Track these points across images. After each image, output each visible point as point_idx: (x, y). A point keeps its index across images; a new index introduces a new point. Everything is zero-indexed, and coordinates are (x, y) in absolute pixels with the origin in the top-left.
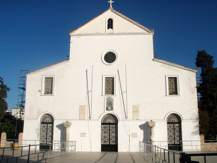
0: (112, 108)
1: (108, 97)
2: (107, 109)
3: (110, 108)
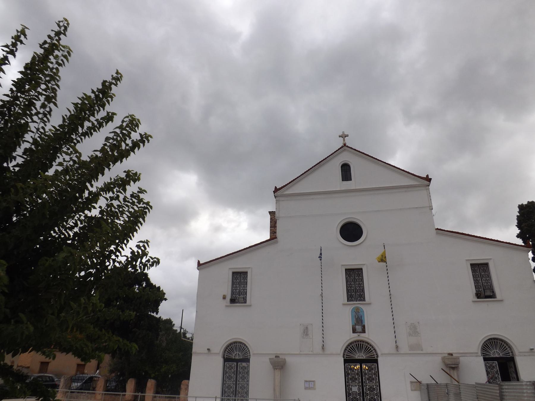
0: (364, 327)
1: (354, 306)
2: (354, 331)
3: (359, 328)
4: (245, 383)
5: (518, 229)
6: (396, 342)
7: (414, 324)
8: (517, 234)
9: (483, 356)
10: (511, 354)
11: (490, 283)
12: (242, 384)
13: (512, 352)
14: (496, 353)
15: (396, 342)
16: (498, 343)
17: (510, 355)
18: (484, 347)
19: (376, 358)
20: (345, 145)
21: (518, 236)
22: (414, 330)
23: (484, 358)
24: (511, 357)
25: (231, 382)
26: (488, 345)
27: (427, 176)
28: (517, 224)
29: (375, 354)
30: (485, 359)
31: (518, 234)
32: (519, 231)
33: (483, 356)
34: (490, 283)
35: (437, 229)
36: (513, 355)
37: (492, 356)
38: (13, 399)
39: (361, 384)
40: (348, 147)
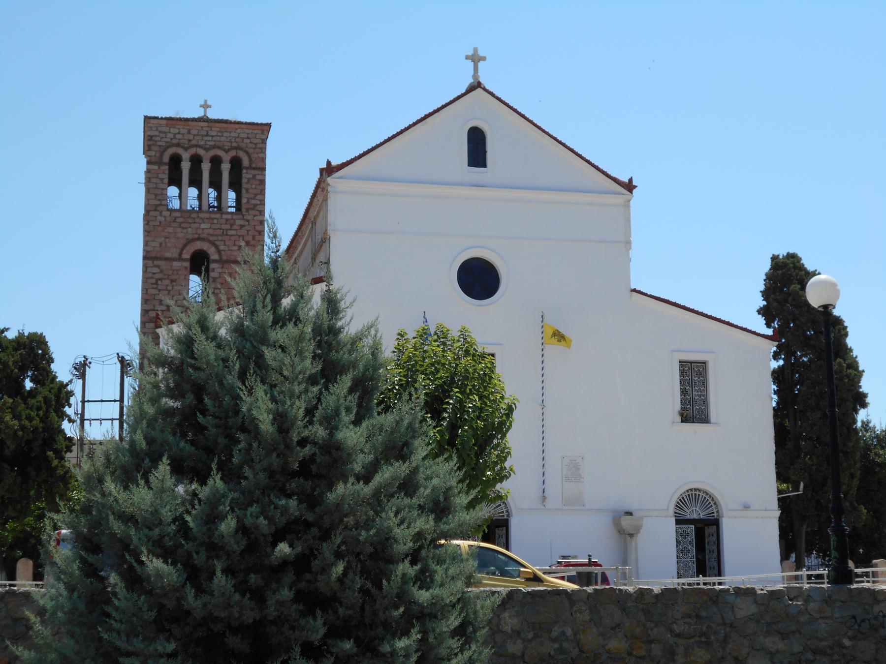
4: (689, 560)
5: (763, 298)
6: (544, 492)
7: (575, 461)
8: (758, 308)
9: (676, 516)
10: (715, 514)
11: (704, 415)
12: (688, 558)
13: (718, 512)
14: (695, 512)
15: (544, 492)
16: (700, 497)
17: (714, 516)
18: (678, 503)
19: (505, 517)
20: (476, 86)
21: (763, 311)
22: (574, 471)
23: (676, 520)
24: (715, 519)
25: (689, 560)
26: (686, 499)
27: (631, 180)
28: (763, 298)
29: (504, 510)
30: (679, 522)
31: (761, 308)
32: (765, 303)
33: (676, 516)
34: (704, 396)
35: (634, 290)
36: (718, 516)
37: (688, 517)
38: (779, 550)
39: (695, 560)
40: (485, 89)
